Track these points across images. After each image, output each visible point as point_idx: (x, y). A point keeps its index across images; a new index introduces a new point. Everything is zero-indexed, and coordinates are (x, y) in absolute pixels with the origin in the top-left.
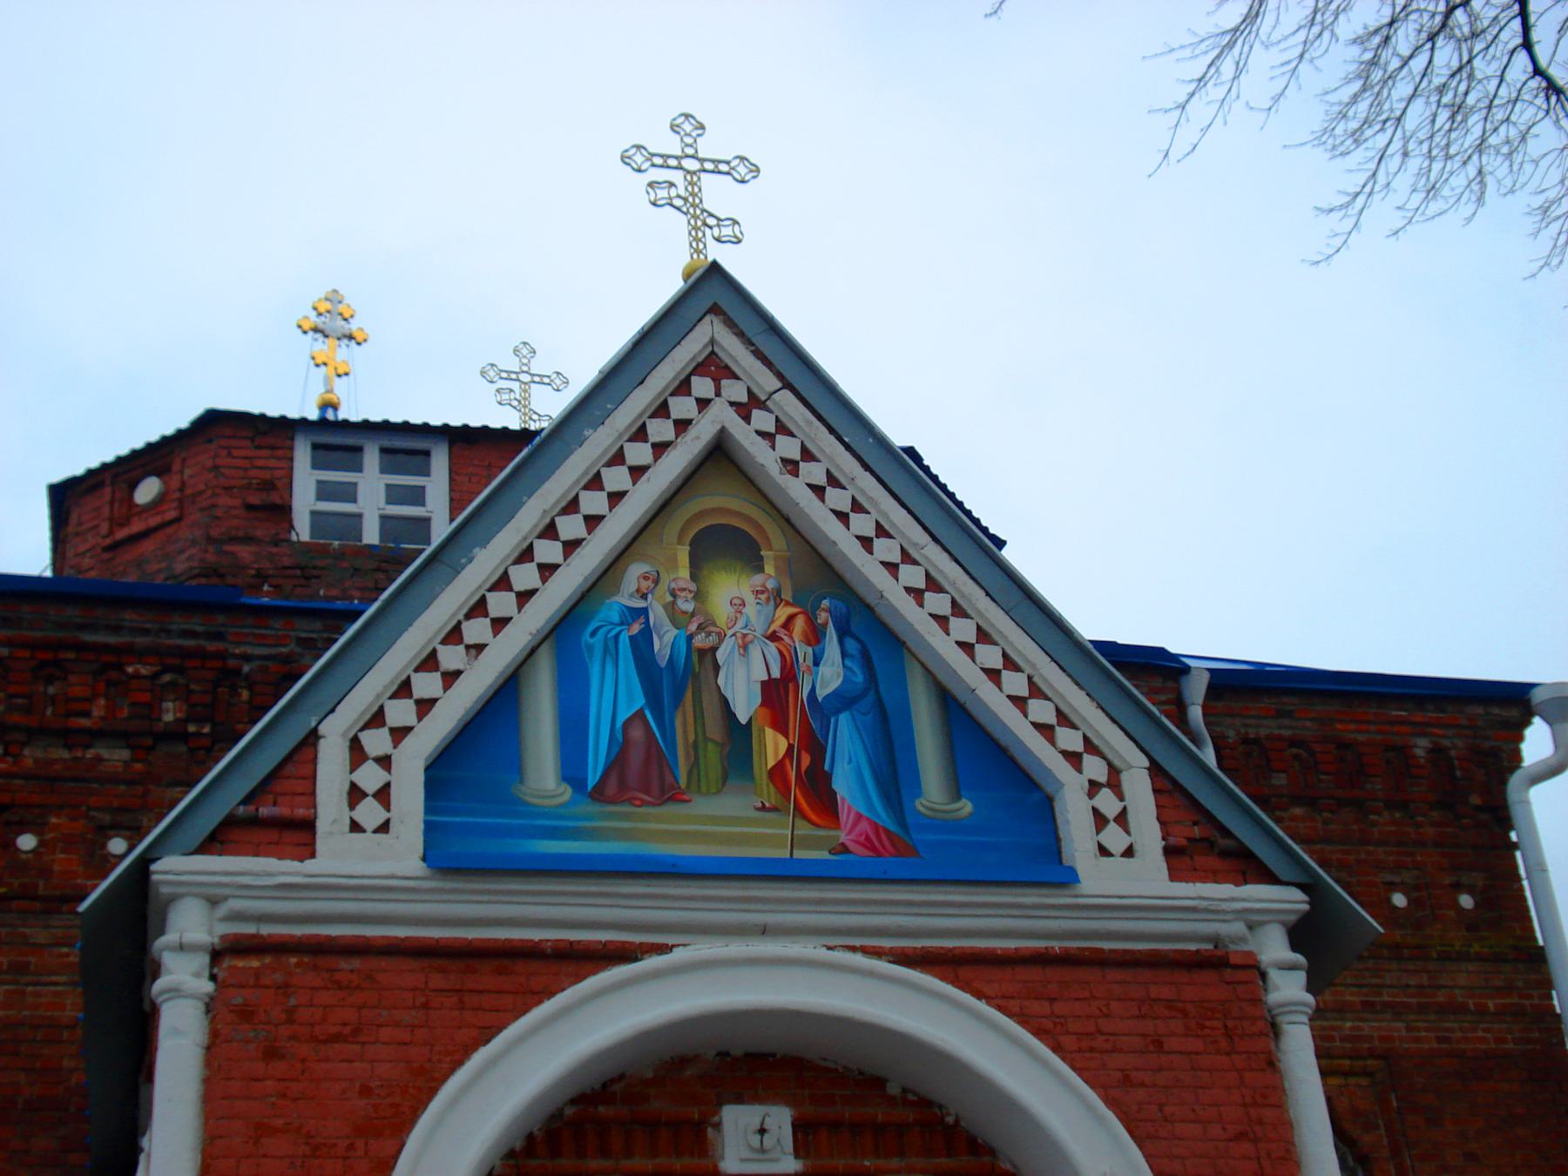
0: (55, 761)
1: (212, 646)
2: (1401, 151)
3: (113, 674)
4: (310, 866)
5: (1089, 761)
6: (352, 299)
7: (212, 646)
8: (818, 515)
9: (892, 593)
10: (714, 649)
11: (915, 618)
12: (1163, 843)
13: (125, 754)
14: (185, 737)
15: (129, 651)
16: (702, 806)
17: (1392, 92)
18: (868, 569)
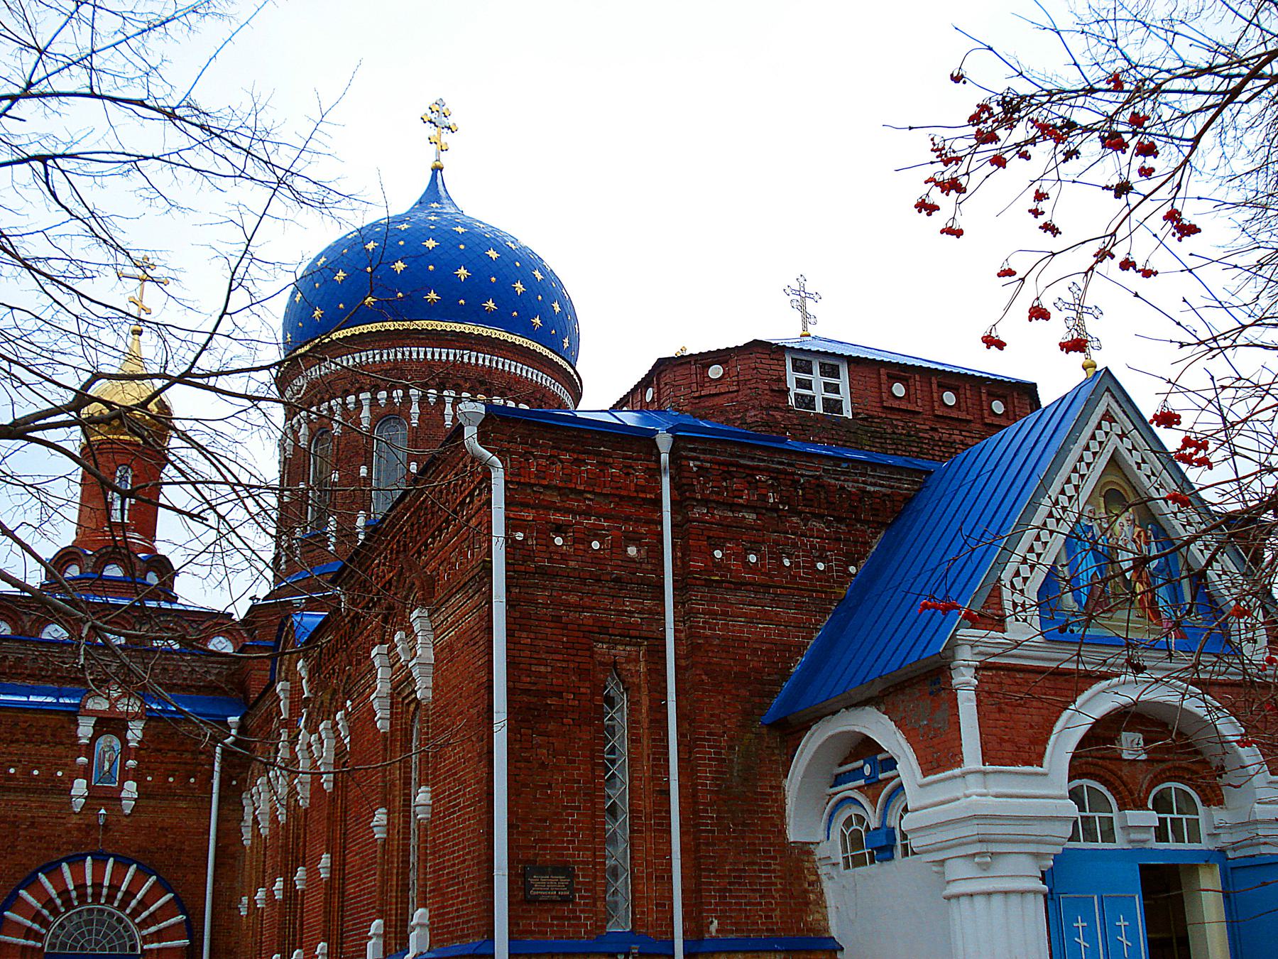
0: (727, 517)
1: (790, 469)
2: (1024, 88)
3: (749, 479)
6: (450, 105)
7: (790, 469)
13: (755, 516)
14: (777, 510)
15: (757, 468)
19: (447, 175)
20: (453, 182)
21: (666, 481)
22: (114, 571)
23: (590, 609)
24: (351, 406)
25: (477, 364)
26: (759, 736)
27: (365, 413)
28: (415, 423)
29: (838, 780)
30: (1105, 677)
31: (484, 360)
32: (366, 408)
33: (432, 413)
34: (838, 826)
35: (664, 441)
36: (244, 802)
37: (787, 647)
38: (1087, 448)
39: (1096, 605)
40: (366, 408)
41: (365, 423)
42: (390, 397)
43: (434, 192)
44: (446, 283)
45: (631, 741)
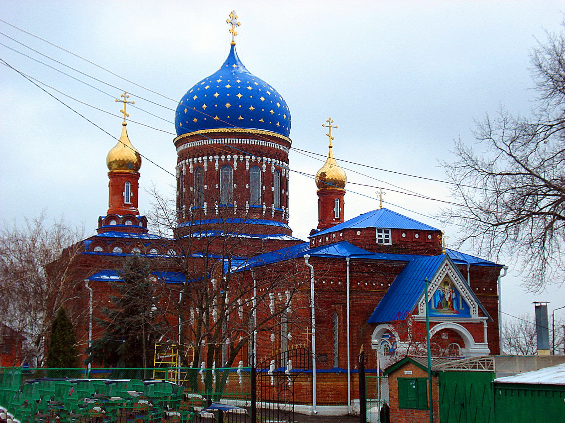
4: (418, 316)
5: (474, 305)
6: (237, 13)
8: (454, 281)
9: (459, 288)
10: (537, 349)
11: (461, 291)
12: (139, 172)
16: (444, 309)
17: (513, 158)
18: (457, 286)
19: (237, 48)
20: (240, 53)
21: (348, 268)
22: (129, 223)
23: (331, 298)
24: (211, 160)
25: (257, 145)
26: (367, 326)
27: (217, 164)
28: (235, 168)
29: (383, 336)
30: (439, 323)
31: (260, 143)
32: (217, 162)
33: (242, 164)
34: (383, 346)
35: (348, 259)
36: (191, 311)
37: (373, 305)
38: (441, 273)
39: (440, 307)
40: (217, 162)
41: (217, 169)
42: (226, 158)
43: (232, 59)
44: (246, 113)
45: (339, 327)
